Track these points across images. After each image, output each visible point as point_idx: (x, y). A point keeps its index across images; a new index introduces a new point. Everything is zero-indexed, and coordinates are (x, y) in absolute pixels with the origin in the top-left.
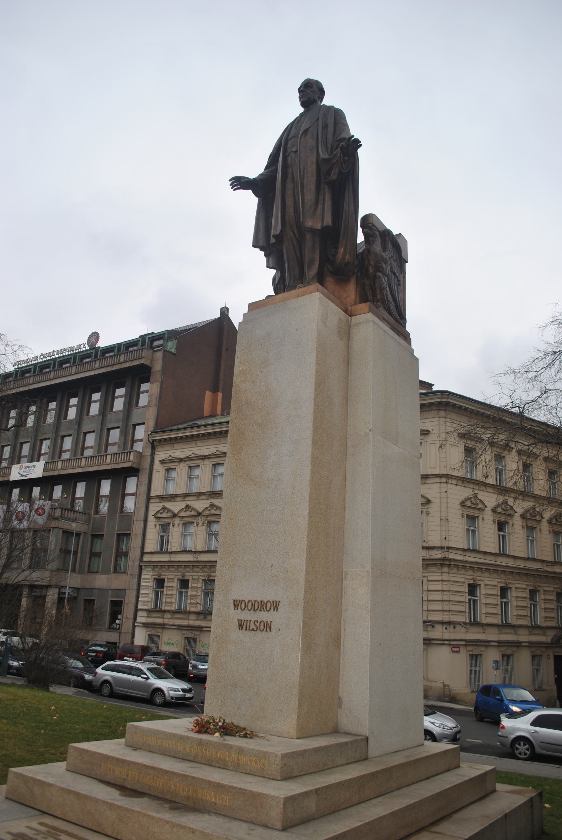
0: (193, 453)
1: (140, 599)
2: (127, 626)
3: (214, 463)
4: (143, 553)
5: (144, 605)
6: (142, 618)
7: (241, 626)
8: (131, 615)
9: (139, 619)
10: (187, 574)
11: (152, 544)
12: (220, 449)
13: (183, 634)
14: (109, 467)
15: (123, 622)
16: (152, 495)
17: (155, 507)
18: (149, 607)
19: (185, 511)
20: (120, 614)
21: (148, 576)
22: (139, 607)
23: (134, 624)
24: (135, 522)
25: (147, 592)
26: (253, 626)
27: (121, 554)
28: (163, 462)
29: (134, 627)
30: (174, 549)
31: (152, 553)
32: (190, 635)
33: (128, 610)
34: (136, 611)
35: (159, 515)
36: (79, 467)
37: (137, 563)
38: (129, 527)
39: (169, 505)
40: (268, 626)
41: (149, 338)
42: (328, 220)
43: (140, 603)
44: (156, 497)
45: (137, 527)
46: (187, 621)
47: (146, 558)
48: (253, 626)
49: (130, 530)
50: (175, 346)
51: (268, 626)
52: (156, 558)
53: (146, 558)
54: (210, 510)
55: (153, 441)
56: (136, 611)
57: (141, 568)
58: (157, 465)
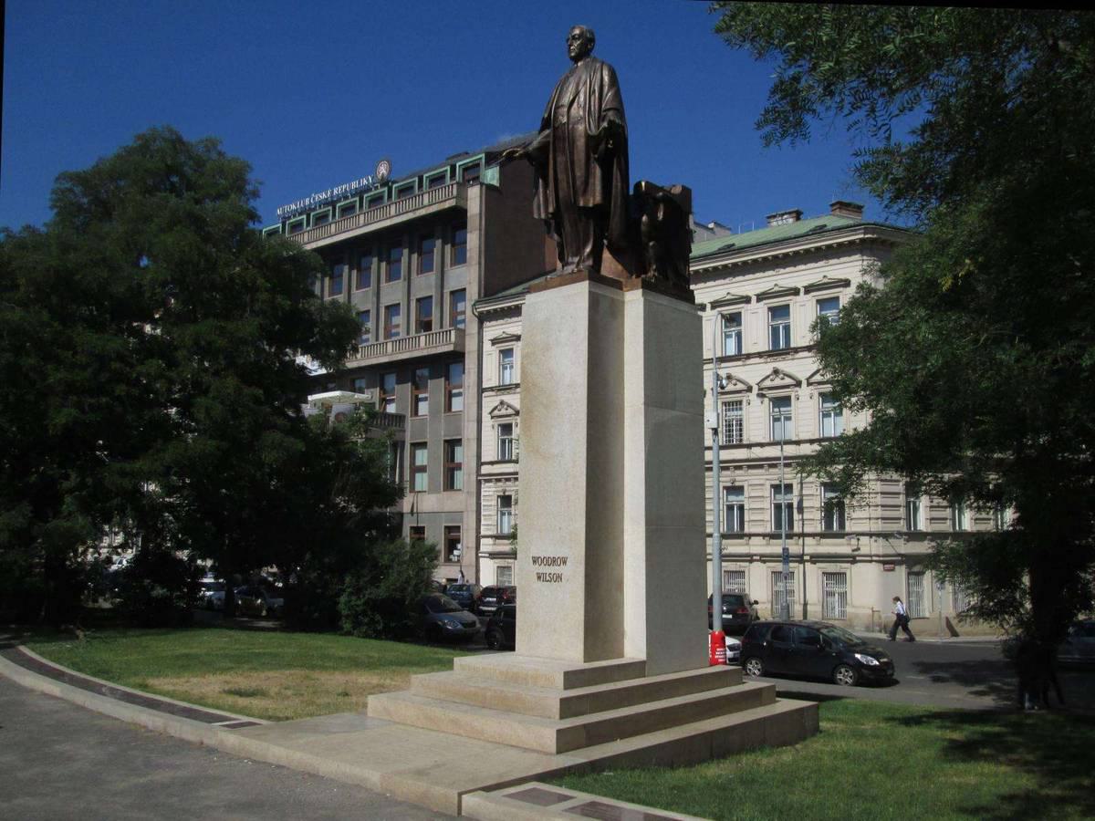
0: (776, 285)
1: (483, 522)
2: (469, 557)
3: (770, 305)
4: (480, 464)
5: (488, 529)
6: (487, 546)
7: (539, 578)
8: (473, 544)
9: (483, 548)
10: (737, 478)
11: (490, 452)
12: (732, 291)
13: (819, 568)
14: (425, 353)
15: (464, 552)
16: (484, 386)
17: (490, 402)
18: (495, 533)
19: (772, 380)
20: (459, 542)
21: (490, 492)
22: (483, 533)
23: (477, 554)
24: (466, 424)
25: (490, 513)
26: (548, 578)
27: (451, 468)
28: (494, 342)
29: (477, 558)
30: (754, 440)
31: (492, 463)
32: (832, 567)
33: (467, 537)
34: (478, 537)
35: (496, 412)
36: (386, 354)
37: (474, 477)
38: (459, 429)
39: (508, 398)
40: (559, 578)
41: (427, 177)
42: (598, 199)
43: (482, 528)
44: (491, 389)
45: (469, 432)
46: (747, 547)
47: (485, 469)
48: (548, 578)
49: (460, 434)
50: (497, 176)
51: (559, 578)
52: (726, 455)
53: (485, 470)
54: (499, 410)
55: (481, 313)
56: (478, 537)
57: (479, 483)
58: (487, 346)
